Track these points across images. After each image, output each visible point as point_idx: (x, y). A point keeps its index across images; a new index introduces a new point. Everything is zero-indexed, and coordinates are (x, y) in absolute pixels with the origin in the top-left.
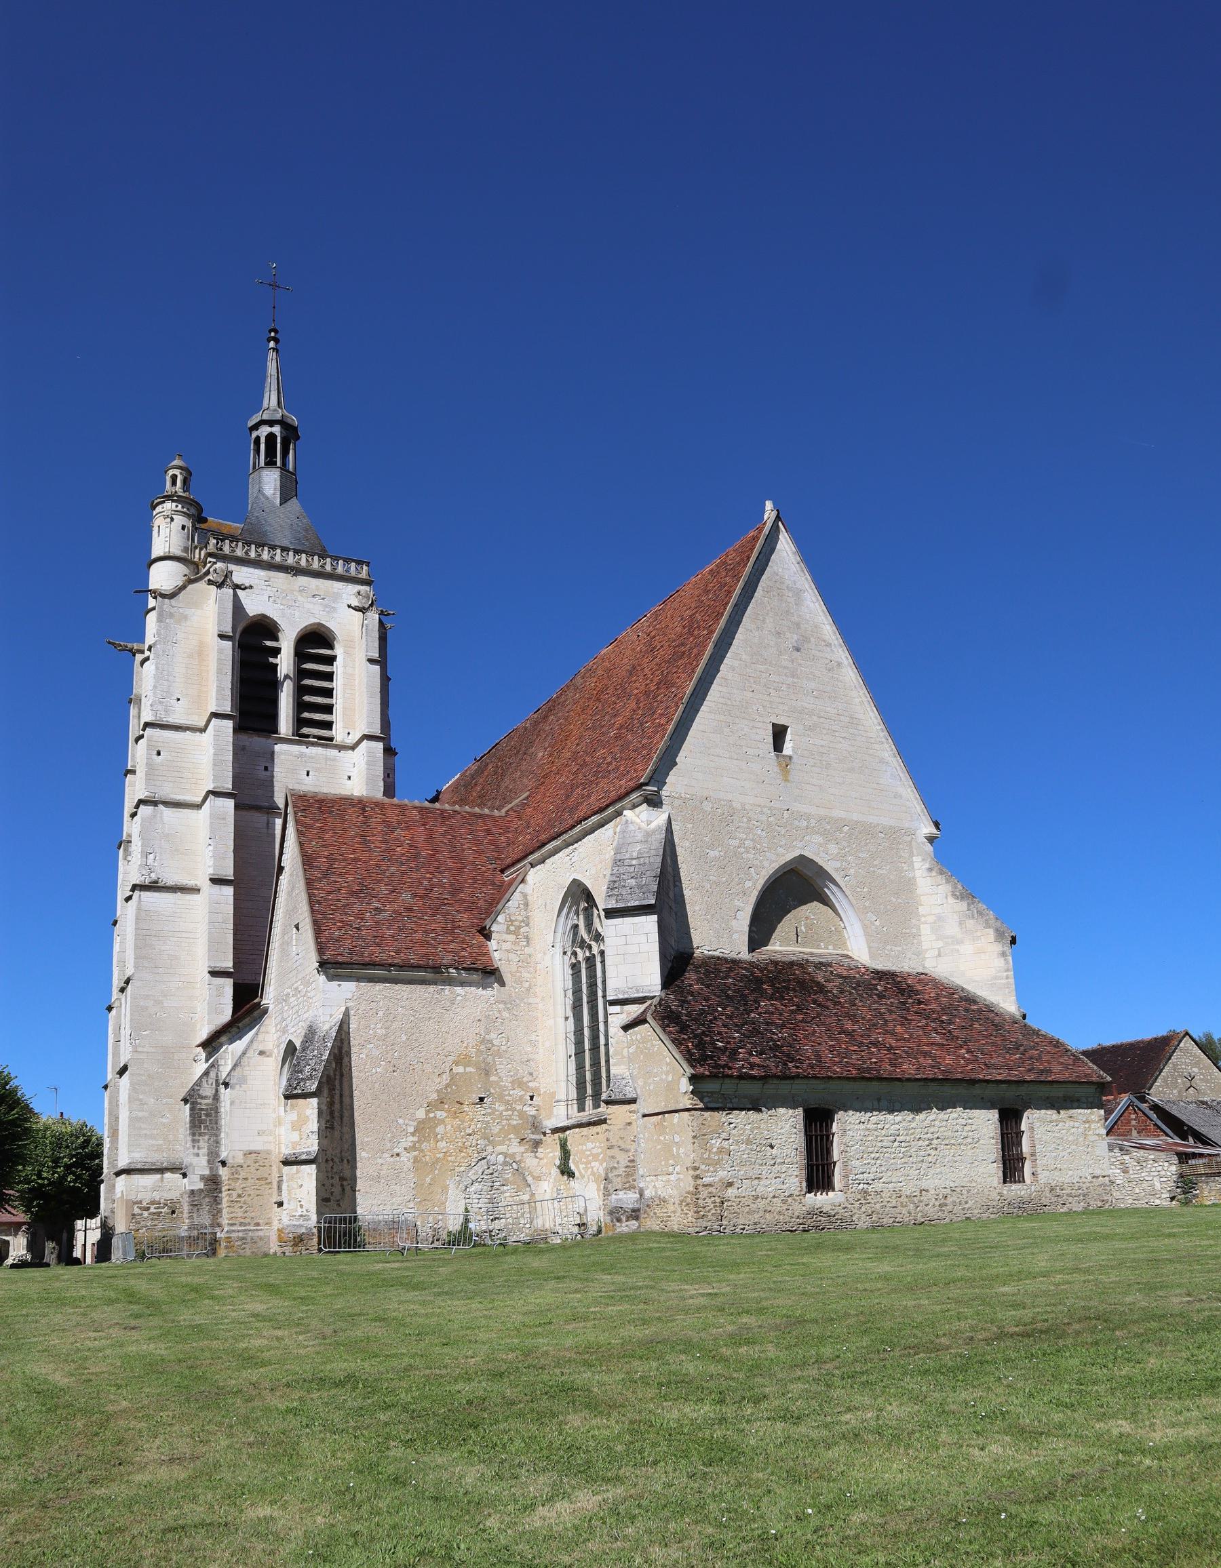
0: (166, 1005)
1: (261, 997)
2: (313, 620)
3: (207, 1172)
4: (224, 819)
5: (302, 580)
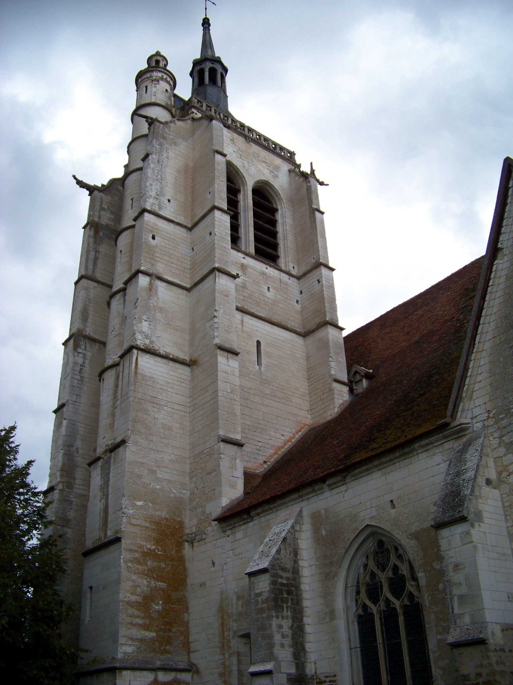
0: (159, 476)
1: (453, 416)
2: (263, 178)
3: (293, 670)
4: (227, 296)
5: (255, 148)
